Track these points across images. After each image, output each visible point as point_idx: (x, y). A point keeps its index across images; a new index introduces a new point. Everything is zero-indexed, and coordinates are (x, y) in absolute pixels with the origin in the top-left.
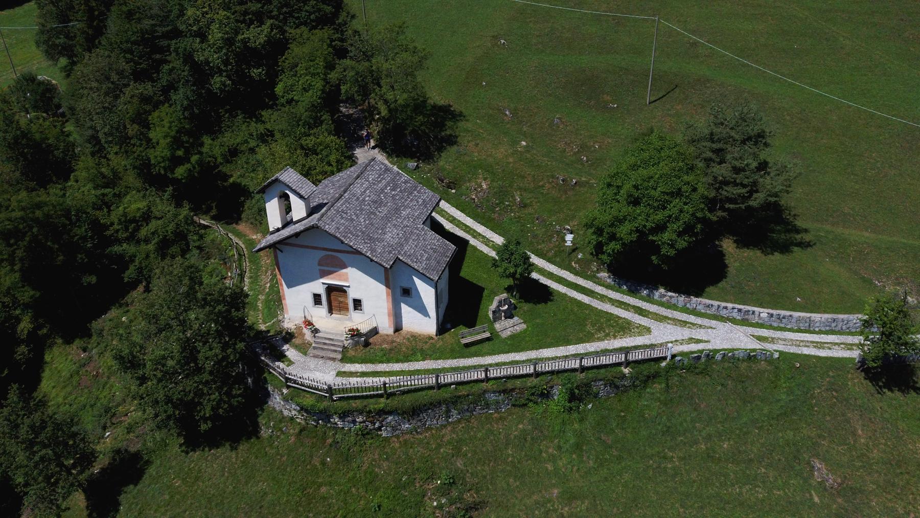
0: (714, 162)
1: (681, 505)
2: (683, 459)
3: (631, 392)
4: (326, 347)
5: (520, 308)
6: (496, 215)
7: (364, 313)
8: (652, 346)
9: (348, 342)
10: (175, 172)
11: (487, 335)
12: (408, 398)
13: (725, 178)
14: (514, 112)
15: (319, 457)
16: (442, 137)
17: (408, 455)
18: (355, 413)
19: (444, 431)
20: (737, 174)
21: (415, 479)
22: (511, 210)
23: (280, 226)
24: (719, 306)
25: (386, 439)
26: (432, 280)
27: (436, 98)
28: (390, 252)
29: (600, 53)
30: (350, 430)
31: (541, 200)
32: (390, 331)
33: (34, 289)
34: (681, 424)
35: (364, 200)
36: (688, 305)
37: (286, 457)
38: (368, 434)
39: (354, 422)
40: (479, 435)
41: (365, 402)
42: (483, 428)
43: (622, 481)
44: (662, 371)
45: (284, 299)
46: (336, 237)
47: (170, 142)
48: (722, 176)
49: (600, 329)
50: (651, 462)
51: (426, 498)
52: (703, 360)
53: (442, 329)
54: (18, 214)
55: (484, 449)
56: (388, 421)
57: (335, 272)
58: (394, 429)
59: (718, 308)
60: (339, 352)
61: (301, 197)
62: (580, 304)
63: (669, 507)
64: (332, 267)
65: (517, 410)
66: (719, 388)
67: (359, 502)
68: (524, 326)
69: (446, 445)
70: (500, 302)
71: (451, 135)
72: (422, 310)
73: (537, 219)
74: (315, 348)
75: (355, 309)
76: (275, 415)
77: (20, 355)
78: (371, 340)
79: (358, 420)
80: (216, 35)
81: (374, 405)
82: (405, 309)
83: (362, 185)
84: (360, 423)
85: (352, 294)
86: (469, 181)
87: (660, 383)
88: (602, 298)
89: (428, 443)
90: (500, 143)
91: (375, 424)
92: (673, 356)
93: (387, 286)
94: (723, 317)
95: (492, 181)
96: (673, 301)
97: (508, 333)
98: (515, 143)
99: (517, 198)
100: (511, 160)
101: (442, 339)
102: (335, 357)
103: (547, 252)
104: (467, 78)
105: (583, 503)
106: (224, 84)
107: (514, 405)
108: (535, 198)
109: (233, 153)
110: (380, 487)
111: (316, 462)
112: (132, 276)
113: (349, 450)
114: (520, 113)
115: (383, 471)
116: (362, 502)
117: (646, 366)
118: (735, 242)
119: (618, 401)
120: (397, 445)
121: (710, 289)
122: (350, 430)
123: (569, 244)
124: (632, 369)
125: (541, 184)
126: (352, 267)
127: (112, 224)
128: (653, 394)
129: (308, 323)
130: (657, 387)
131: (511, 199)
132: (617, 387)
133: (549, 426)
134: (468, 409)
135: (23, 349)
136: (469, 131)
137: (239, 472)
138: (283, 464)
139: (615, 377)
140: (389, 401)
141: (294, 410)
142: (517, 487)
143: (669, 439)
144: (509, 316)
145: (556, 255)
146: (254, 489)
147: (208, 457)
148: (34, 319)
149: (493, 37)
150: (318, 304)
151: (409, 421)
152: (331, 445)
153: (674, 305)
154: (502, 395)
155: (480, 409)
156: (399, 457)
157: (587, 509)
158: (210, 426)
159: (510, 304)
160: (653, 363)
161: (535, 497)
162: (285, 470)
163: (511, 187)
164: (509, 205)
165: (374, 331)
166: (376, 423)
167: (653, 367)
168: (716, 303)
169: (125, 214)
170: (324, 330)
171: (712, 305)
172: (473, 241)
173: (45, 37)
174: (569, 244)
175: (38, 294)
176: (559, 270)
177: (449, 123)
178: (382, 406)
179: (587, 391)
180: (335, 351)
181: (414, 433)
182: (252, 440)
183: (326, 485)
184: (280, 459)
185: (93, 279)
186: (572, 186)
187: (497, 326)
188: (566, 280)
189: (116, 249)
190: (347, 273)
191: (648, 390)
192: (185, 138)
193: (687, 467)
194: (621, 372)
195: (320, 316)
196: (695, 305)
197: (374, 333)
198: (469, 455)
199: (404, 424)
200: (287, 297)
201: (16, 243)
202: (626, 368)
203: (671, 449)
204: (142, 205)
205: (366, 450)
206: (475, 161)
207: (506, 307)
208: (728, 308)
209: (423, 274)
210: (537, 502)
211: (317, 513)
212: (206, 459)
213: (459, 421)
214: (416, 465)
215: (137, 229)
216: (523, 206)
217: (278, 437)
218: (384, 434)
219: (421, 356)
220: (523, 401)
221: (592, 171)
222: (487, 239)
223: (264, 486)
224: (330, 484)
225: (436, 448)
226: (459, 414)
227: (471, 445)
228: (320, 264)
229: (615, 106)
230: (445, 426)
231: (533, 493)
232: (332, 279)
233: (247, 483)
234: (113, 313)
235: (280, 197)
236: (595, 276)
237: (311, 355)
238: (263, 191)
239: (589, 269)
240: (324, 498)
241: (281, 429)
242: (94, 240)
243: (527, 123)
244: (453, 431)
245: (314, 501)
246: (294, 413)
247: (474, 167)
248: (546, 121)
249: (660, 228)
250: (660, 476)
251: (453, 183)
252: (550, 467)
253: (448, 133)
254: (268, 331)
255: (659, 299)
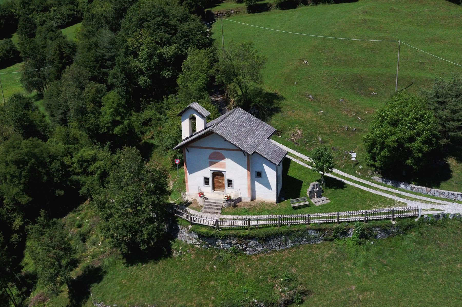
0: (439, 109)
1: (433, 296)
2: (432, 272)
3: (397, 237)
4: (212, 207)
5: (326, 192)
6: (307, 148)
7: (233, 189)
8: (408, 211)
9: (225, 203)
10: (114, 130)
11: (307, 203)
12: (262, 231)
13: (447, 117)
14: (315, 97)
15: (209, 265)
16: (272, 109)
17: (262, 265)
18: (232, 238)
19: (283, 253)
20: (453, 114)
21: (267, 278)
22: (316, 145)
23: (189, 136)
24: (449, 193)
25: (248, 256)
26: (275, 164)
27: (267, 88)
28: (251, 148)
29: (365, 67)
30: (228, 250)
31: (335, 139)
32: (249, 200)
33: (29, 196)
34: (430, 255)
35: (234, 124)
36: (429, 193)
37: (189, 266)
38: (238, 252)
39: (230, 244)
40: (305, 256)
41: (238, 231)
42: (307, 252)
43: (395, 283)
44: (415, 224)
45: (187, 182)
46: (222, 137)
47: (113, 111)
48: (445, 116)
49: (375, 204)
50: (412, 274)
51: (275, 288)
52: (441, 218)
53: (279, 199)
54: (26, 150)
55: (308, 263)
56: (251, 244)
57: (218, 162)
58: (254, 250)
59: (448, 194)
60: (220, 209)
61: (202, 116)
62: (362, 191)
63: (425, 297)
64: (217, 159)
65: (327, 243)
66: (452, 234)
67: (234, 289)
68: (329, 201)
69: (285, 260)
70: (314, 186)
71: (277, 107)
72: (268, 186)
73: (333, 149)
74: (205, 208)
75: (228, 187)
76: (182, 243)
77: (14, 239)
78: (237, 204)
79: (233, 242)
80: (143, 52)
81: (242, 233)
82: (258, 185)
83: (233, 117)
84: (234, 244)
85: (227, 176)
86: (290, 130)
87: (415, 232)
88: (376, 189)
89: (274, 259)
90: (307, 111)
91: (242, 246)
92: (422, 216)
93: (248, 170)
94: (452, 200)
95: (304, 130)
96: (420, 191)
97: (320, 204)
98: (316, 111)
99: (320, 138)
100: (315, 119)
101: (280, 205)
102: (217, 212)
103: (340, 166)
104: (286, 80)
105: (371, 293)
106: (146, 82)
107: (325, 240)
108: (331, 138)
109: (147, 123)
110: (247, 282)
111: (208, 268)
112: (84, 192)
113: (227, 261)
114: (319, 97)
115: (248, 273)
116: (236, 289)
117: (406, 220)
118: (456, 160)
119: (389, 241)
120: (256, 260)
121: (443, 184)
122: (228, 250)
123: (353, 159)
124: (397, 221)
125: (334, 131)
126: (228, 158)
127: (73, 163)
128: (411, 238)
129: (201, 194)
130: (413, 234)
131: (316, 139)
132: (388, 233)
133: (347, 252)
134: (297, 240)
135: (15, 236)
136: (288, 105)
137: (161, 275)
138: (187, 270)
139: (387, 226)
140: (251, 231)
141: (195, 238)
142: (330, 284)
143: (422, 262)
144: (319, 196)
145: (346, 167)
146: (170, 283)
147: (142, 268)
148: (23, 219)
149: (300, 59)
150: (206, 185)
151: (262, 245)
152: (216, 259)
153: (420, 193)
154: (318, 232)
155: (305, 241)
156: (257, 266)
157: (374, 296)
158: (146, 247)
159: (320, 189)
160: (409, 219)
161: (341, 290)
162: (189, 273)
163: (316, 133)
164: (315, 142)
165: (239, 200)
166: (243, 245)
167: (410, 222)
168: (447, 192)
169: (82, 157)
170: (210, 198)
171: (444, 193)
172: (293, 159)
173: (26, 77)
174: (353, 159)
175: (31, 199)
176: (348, 175)
177: (275, 101)
178: (248, 233)
179: (370, 234)
180: (217, 209)
181: (266, 253)
182: (168, 259)
183: (214, 280)
184: (186, 267)
185: (62, 193)
186: (353, 131)
187: (313, 200)
188: (353, 180)
189: (75, 177)
190: (225, 163)
191: (408, 236)
192: (121, 110)
193: (436, 277)
194: (391, 223)
195: (208, 191)
196: (433, 193)
197: (239, 201)
198: (300, 266)
199: (260, 246)
200: (189, 181)
201: (22, 167)
202: (393, 221)
203: (424, 267)
204: (92, 152)
205: (237, 262)
206: (293, 120)
207: (318, 189)
208: (455, 194)
209: (270, 161)
210: (342, 292)
211: (210, 294)
212: (141, 270)
213: (293, 248)
214: (268, 270)
215: (88, 167)
216: (324, 142)
217: (185, 255)
218: (247, 253)
219: (268, 213)
220: (331, 237)
221: (365, 125)
222: (303, 159)
223: (176, 282)
224: (216, 280)
225: (279, 262)
226: (292, 243)
227: (300, 261)
228: (210, 158)
229: (376, 93)
230: (284, 250)
231: (340, 288)
232: (214, 167)
233: (166, 280)
234: (71, 215)
235: (190, 119)
236: (370, 179)
237: (203, 211)
238: (181, 115)
239: (366, 174)
240: (213, 287)
241: (186, 251)
242: (63, 172)
243: (323, 102)
244: (289, 253)
245: (207, 288)
246: (194, 241)
247: (293, 123)
248: (335, 100)
249: (411, 139)
250: (419, 281)
251: (280, 132)
252: (350, 274)
253: (276, 106)
254: (175, 203)
255: (411, 190)
